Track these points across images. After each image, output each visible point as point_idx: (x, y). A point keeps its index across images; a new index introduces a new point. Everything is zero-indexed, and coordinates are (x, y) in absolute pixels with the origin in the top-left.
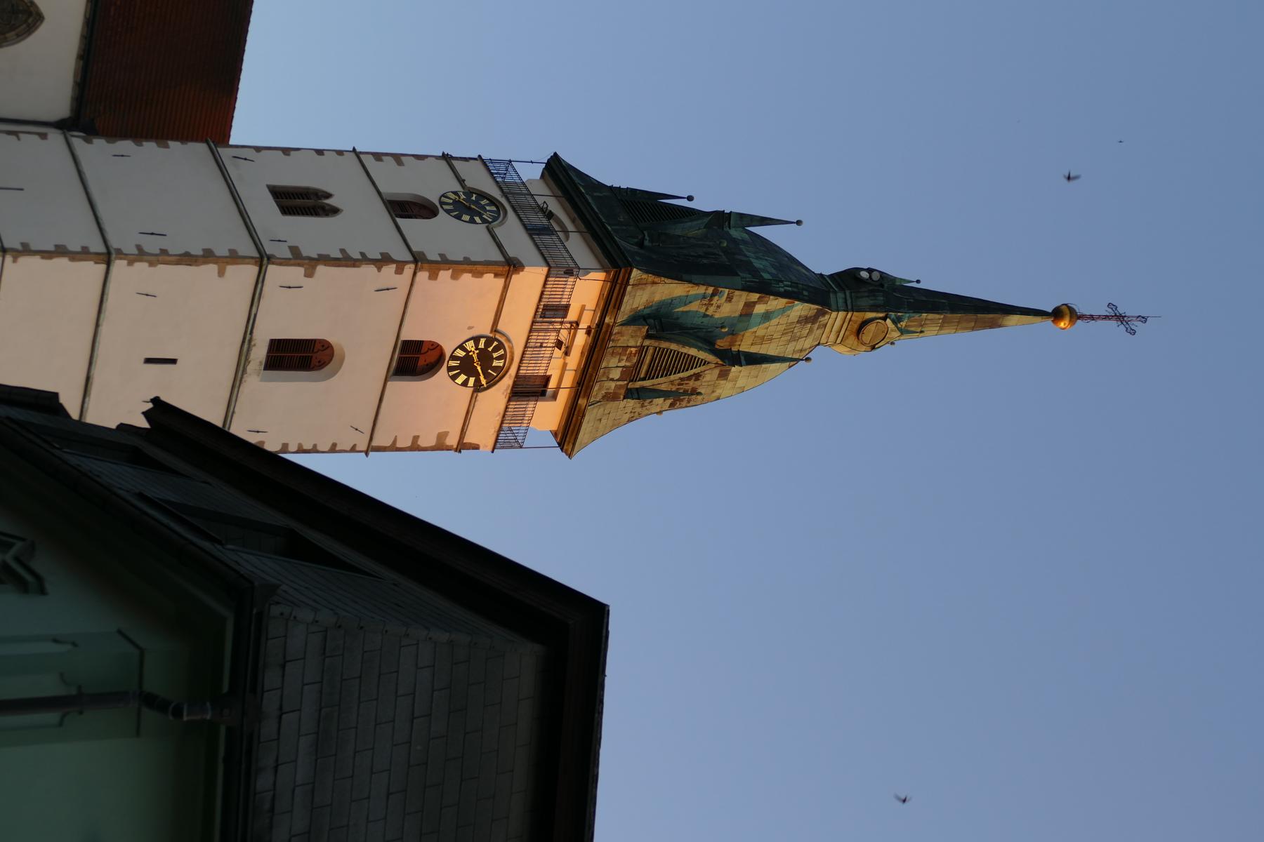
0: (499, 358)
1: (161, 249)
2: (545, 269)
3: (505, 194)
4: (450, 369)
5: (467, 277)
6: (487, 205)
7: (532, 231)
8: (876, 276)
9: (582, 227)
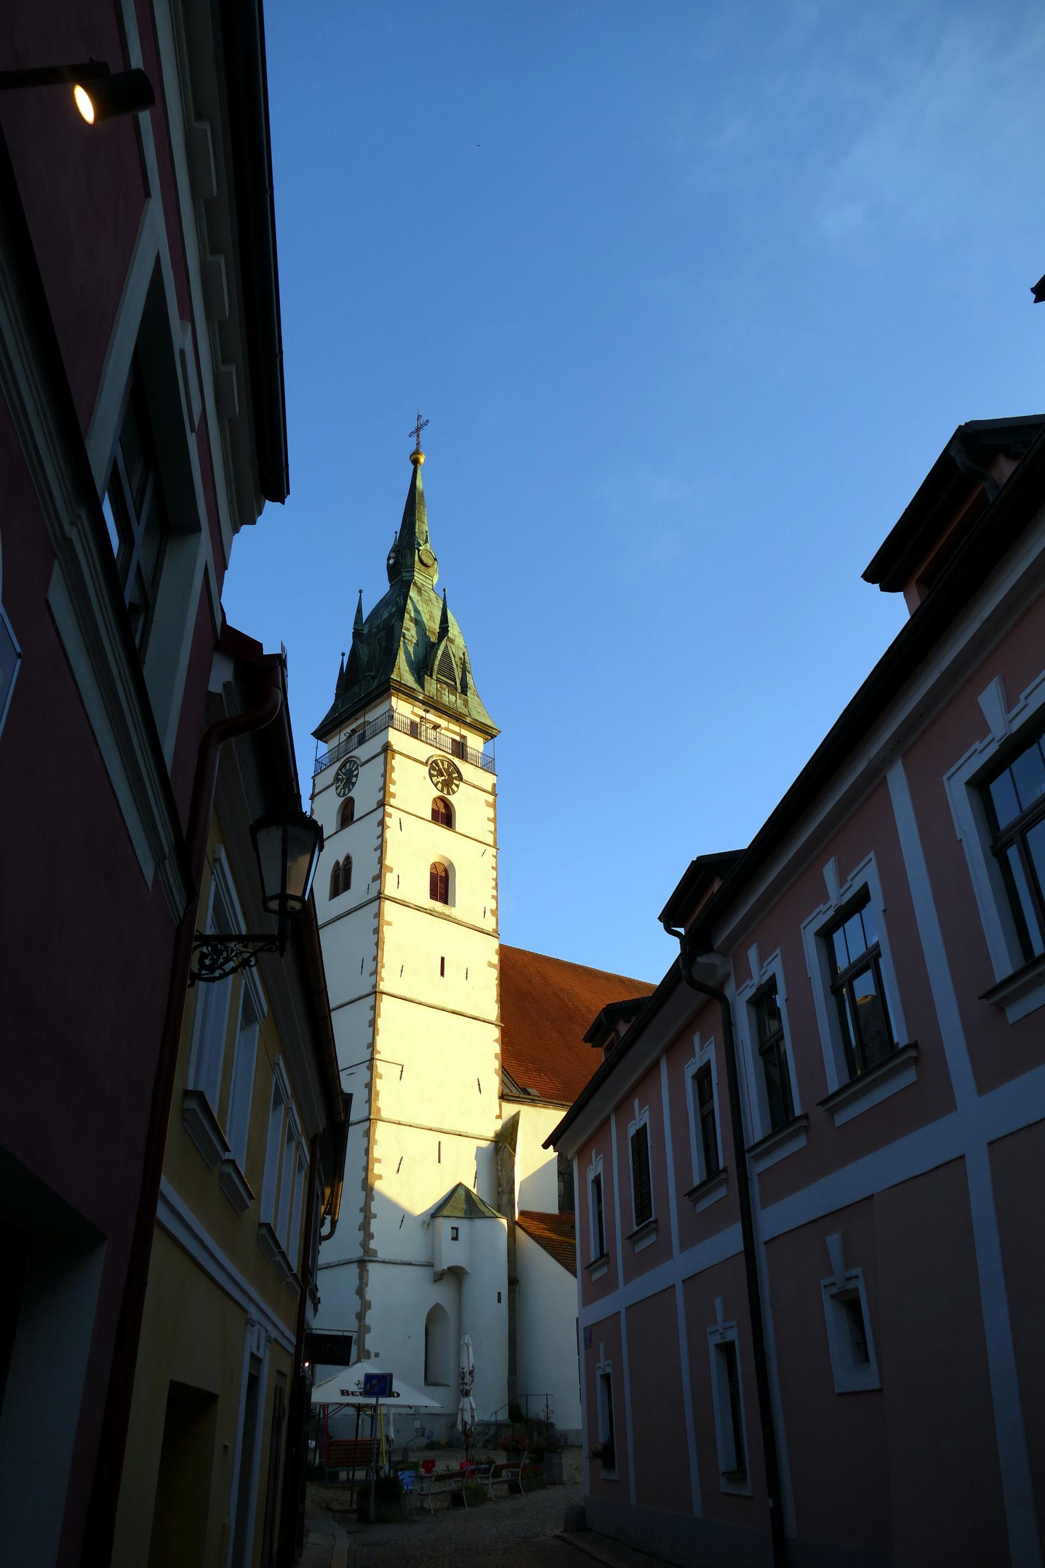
0: (443, 765)
1: (373, 961)
2: (390, 729)
3: (338, 760)
4: (449, 794)
5: (394, 776)
6: (345, 769)
7: (362, 741)
8: (393, 555)
9: (362, 712)
